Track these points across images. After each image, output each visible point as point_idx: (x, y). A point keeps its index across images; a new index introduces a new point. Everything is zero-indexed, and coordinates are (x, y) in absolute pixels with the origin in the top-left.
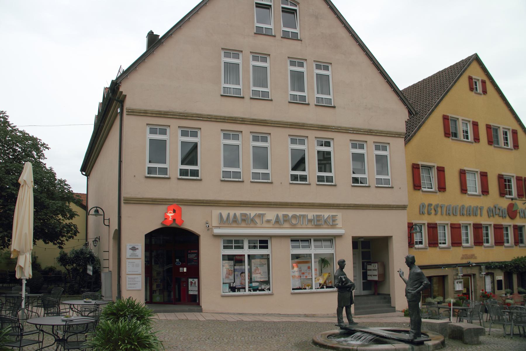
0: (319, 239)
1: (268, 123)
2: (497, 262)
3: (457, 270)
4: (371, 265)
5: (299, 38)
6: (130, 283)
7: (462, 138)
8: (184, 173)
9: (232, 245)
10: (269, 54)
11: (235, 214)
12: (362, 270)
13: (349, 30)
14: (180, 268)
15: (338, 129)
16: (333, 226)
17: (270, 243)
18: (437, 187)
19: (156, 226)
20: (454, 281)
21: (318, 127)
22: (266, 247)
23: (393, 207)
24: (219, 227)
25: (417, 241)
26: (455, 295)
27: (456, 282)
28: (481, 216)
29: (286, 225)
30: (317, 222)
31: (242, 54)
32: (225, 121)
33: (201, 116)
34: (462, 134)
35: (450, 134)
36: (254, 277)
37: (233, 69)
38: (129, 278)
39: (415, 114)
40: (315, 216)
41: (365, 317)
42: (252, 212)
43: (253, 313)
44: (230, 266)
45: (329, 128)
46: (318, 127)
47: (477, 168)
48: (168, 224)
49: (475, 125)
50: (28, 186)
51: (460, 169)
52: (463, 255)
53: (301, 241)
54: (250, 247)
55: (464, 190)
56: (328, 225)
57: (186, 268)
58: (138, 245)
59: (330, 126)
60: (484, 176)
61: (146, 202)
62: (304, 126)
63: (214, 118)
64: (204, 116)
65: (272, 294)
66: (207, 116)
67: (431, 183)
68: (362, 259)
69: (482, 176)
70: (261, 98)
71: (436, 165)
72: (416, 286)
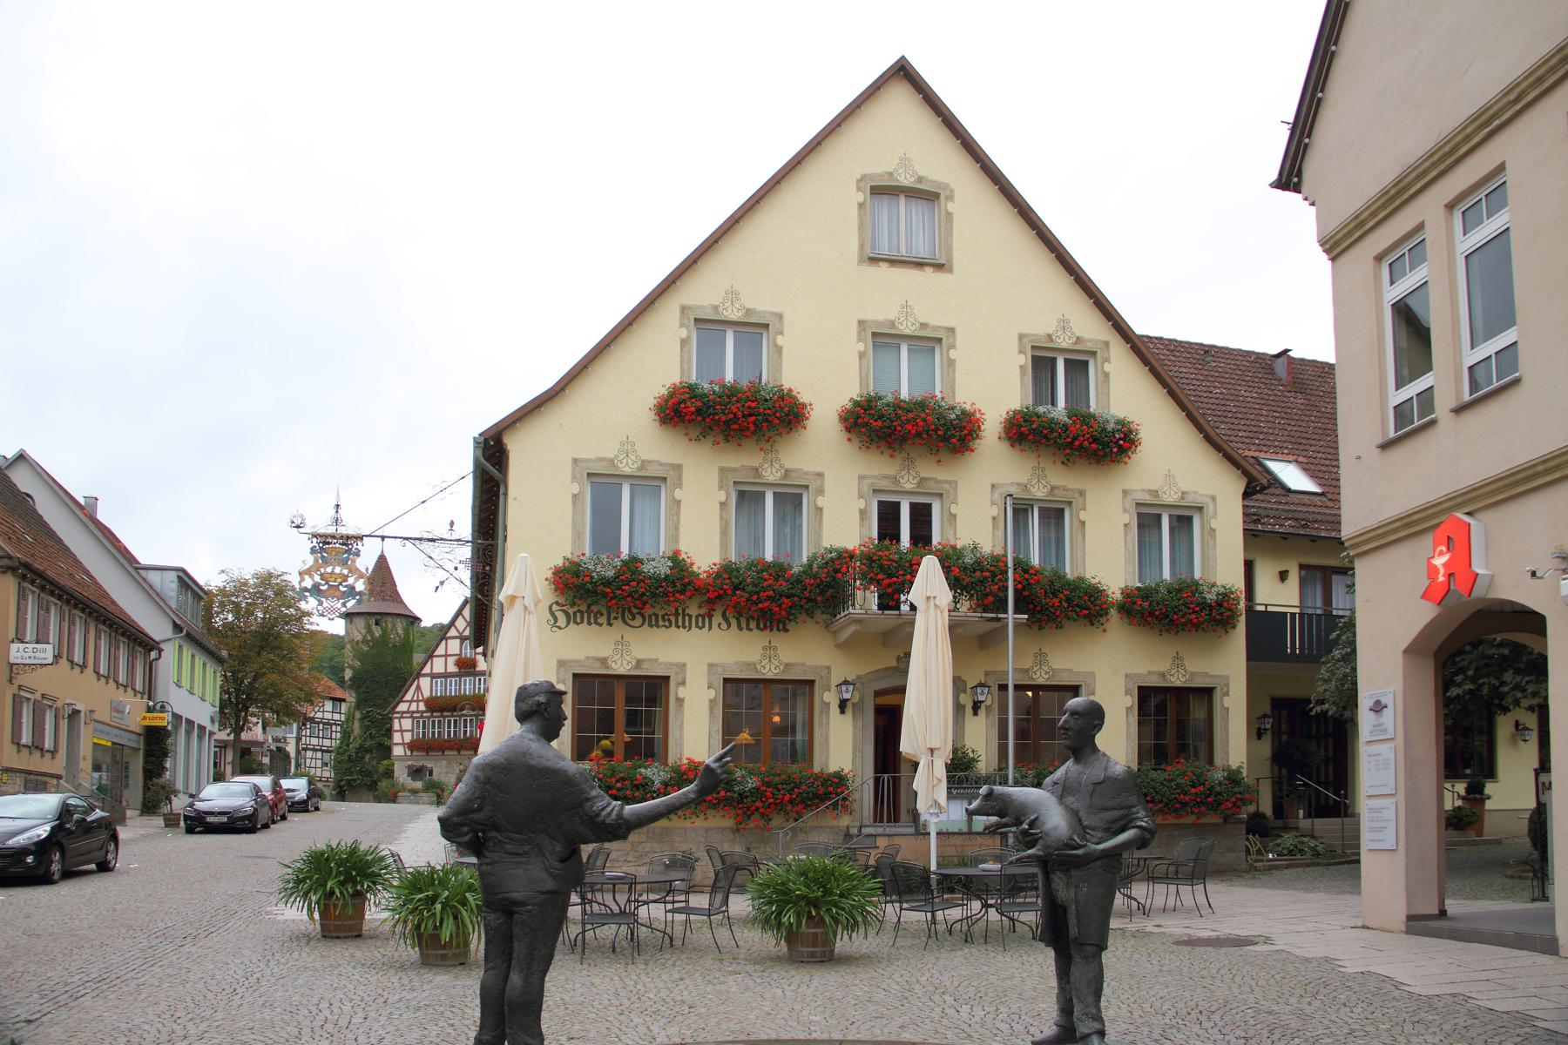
6: (1373, 825)
64: (1495, 108)
66: (1505, 100)
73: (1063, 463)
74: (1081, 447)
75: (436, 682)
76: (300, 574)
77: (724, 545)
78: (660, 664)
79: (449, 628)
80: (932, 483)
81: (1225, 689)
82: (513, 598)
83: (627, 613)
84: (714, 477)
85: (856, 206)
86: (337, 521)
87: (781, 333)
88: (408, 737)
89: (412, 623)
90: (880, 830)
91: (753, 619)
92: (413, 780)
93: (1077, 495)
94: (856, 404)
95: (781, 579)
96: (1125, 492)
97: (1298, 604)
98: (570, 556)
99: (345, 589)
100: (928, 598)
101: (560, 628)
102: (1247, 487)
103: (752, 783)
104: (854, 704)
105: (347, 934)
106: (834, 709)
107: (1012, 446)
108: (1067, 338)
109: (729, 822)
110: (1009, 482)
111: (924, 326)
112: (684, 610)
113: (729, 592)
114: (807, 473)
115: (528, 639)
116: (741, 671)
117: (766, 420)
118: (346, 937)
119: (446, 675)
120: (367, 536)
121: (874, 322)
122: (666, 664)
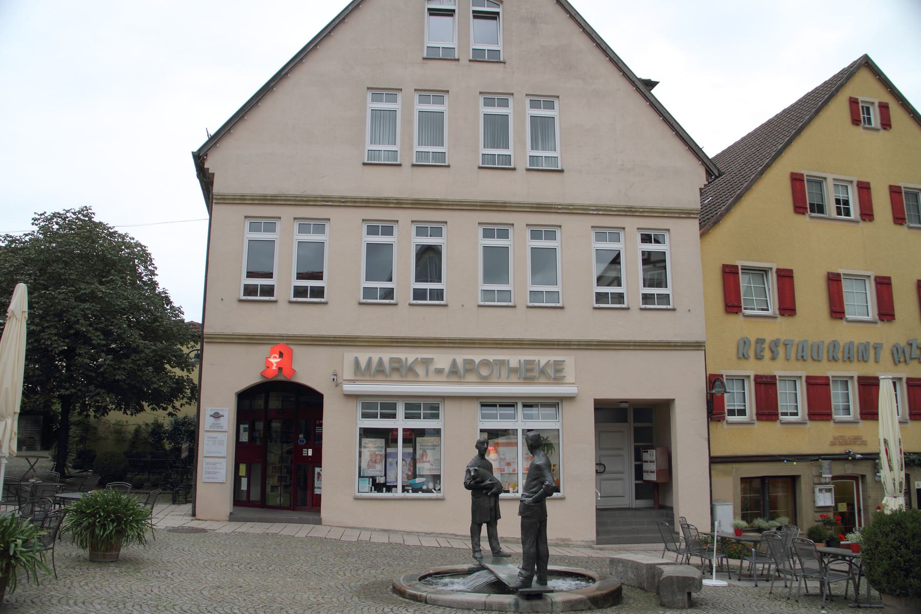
0: (530, 403)
1: (442, 205)
2: (914, 453)
3: (821, 467)
4: (647, 452)
5: (502, 60)
7: (834, 214)
8: (646, 298)
9: (376, 411)
10: (557, 95)
11: (380, 359)
12: (635, 461)
13: (592, 37)
14: (304, 450)
15: (568, 209)
16: (558, 380)
17: (443, 412)
18: (777, 306)
19: (252, 378)
20: (813, 488)
21: (532, 207)
22: (436, 416)
23: (675, 346)
24: (353, 381)
25: (735, 410)
26: (816, 514)
27: (817, 490)
28: (876, 361)
29: (471, 378)
30: (527, 373)
31: (449, 96)
32: (370, 205)
33: (331, 199)
34: (833, 206)
35: (807, 208)
36: (419, 468)
37: (428, 122)
38: (207, 463)
39: (717, 175)
40: (522, 361)
41: (612, 549)
42: (409, 356)
43: (407, 531)
44: (378, 447)
45: (551, 208)
46: (532, 207)
47: (867, 270)
48: (271, 376)
49: (864, 189)
50: (17, 319)
51: (828, 273)
52: (835, 438)
53: (500, 406)
54: (408, 416)
55: (837, 311)
56: (549, 379)
57: (311, 450)
58: (223, 410)
59: (552, 205)
60: (884, 285)
61: (238, 341)
62: (506, 207)
63: (351, 202)
65: (443, 498)
66: (339, 199)
67: (767, 300)
68: (635, 442)
69: (879, 286)
70: (498, 166)
71: (774, 267)
72: (534, 490)
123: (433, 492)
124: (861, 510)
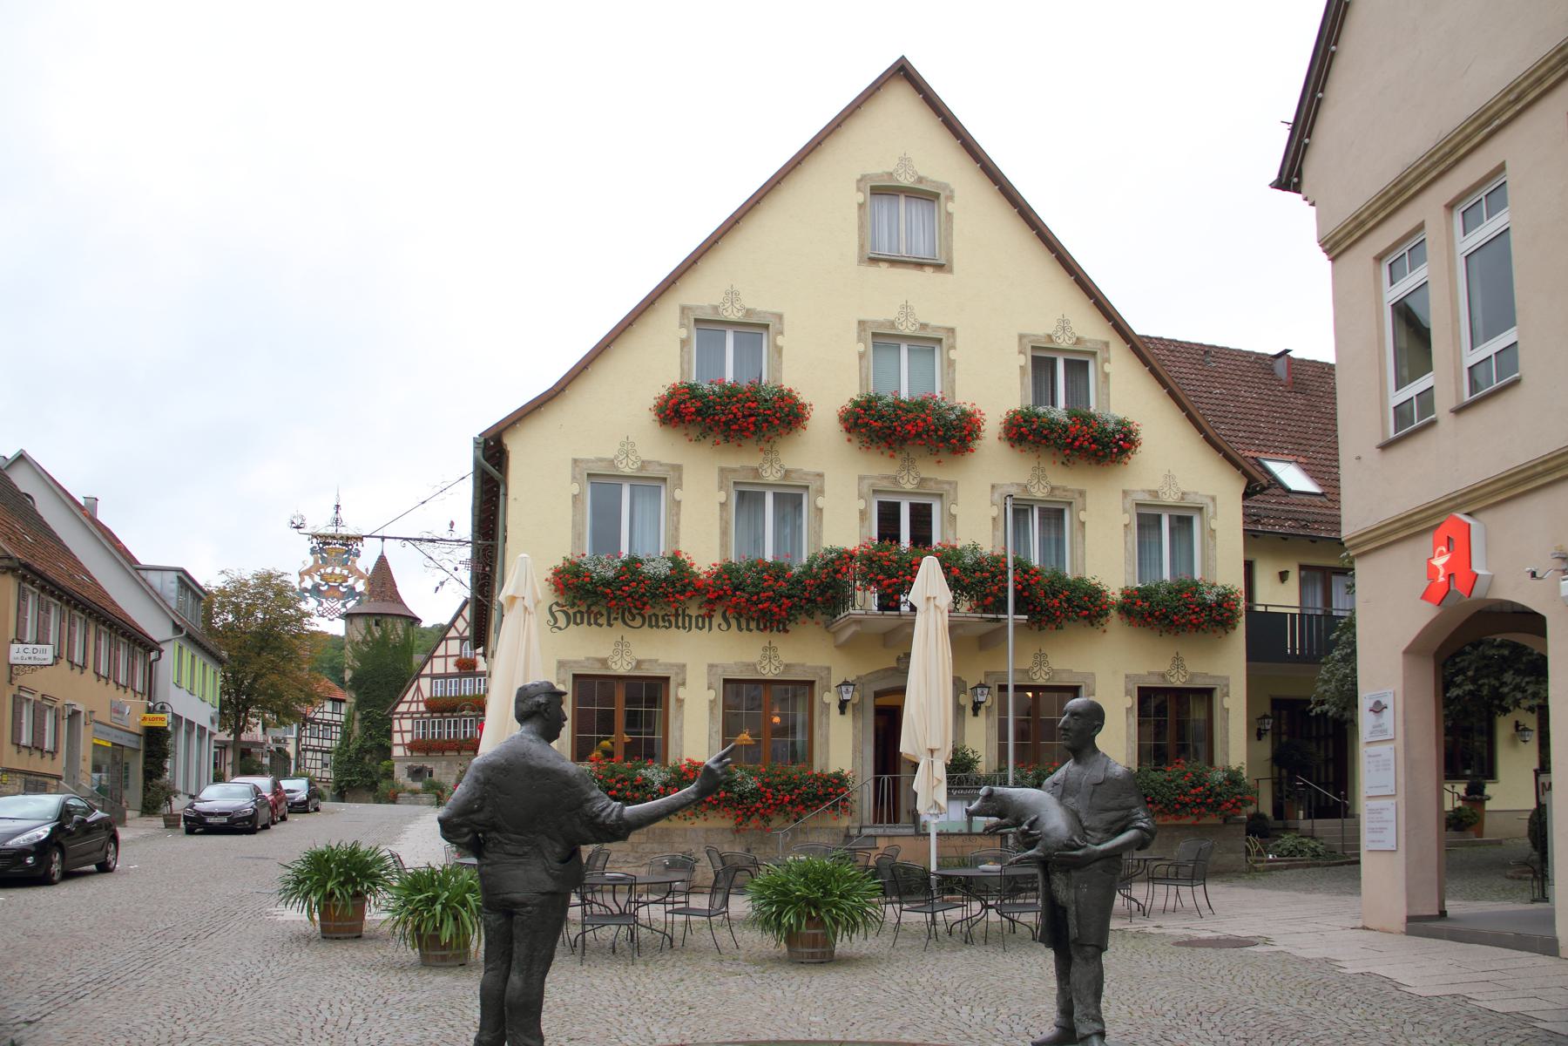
6: (1373, 825)
64: (1495, 108)
66: (1505, 100)
73: (1063, 463)
74: (1081, 447)
75: (436, 683)
76: (300, 574)
77: (724, 546)
78: (660, 665)
79: (449, 629)
80: (932, 484)
81: (1225, 690)
82: (513, 599)
83: (627, 613)
84: (714, 478)
85: (856, 206)
86: (337, 522)
87: (781, 333)
88: (408, 738)
89: (412, 624)
90: (880, 831)
91: (753, 619)
92: (413, 780)
93: (1077, 496)
94: (856, 404)
95: (781, 579)
96: (1125, 493)
97: (1298, 605)
98: (570, 557)
99: (345, 590)
100: (928, 599)
101: (560, 629)
102: (1247, 487)
103: (752, 784)
104: (854, 705)
105: (347, 935)
106: (834, 709)
107: (1012, 446)
108: (1067, 338)
109: (729, 823)
110: (1009, 483)
111: (924, 326)
112: (684, 611)
113: (729, 592)
114: (807, 474)
115: (528, 640)
116: (741, 671)
117: (766, 421)
118: (346, 938)
119: (446, 676)
120: (367, 536)
121: (874, 322)
122: (666, 665)
123: (382, 563)
124: (1491, 124)
